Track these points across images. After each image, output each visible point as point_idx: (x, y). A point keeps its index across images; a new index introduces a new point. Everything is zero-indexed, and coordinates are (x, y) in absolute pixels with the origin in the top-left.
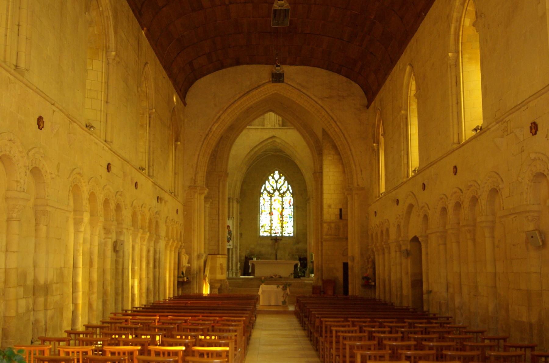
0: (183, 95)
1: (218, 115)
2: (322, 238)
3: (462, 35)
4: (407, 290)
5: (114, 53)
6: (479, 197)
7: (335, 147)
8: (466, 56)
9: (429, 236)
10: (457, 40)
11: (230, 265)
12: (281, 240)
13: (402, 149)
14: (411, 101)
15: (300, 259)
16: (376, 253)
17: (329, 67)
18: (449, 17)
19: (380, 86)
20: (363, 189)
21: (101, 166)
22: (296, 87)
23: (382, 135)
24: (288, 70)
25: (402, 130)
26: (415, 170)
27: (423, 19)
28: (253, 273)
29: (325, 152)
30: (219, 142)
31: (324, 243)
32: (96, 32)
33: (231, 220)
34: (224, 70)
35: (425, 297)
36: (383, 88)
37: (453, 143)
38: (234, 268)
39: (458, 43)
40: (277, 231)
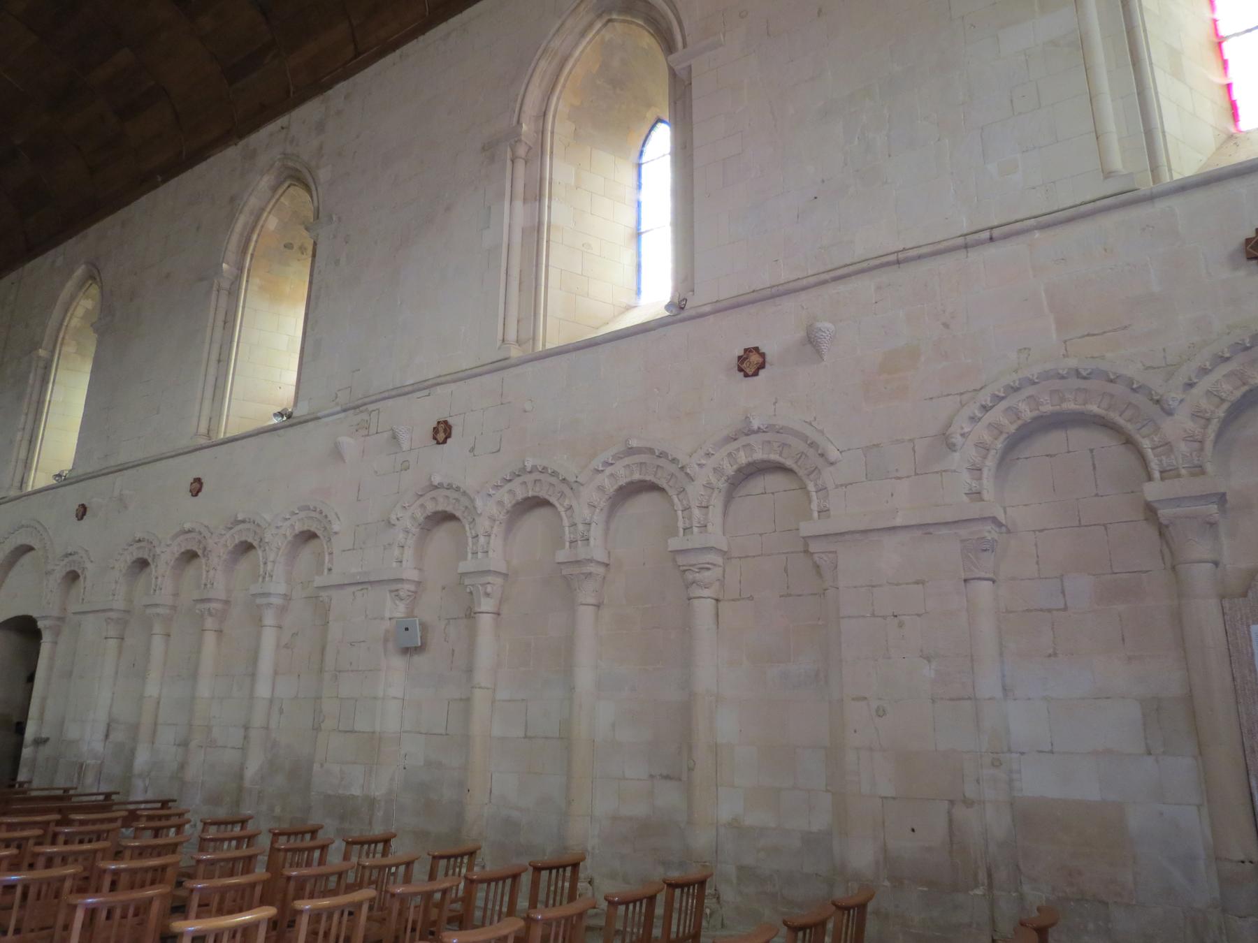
3: (256, 241)
8: (256, 281)
13: (21, 426)
14: (67, 337)
25: (29, 390)
27: (156, 187)
35: (27, 752)
37: (197, 434)
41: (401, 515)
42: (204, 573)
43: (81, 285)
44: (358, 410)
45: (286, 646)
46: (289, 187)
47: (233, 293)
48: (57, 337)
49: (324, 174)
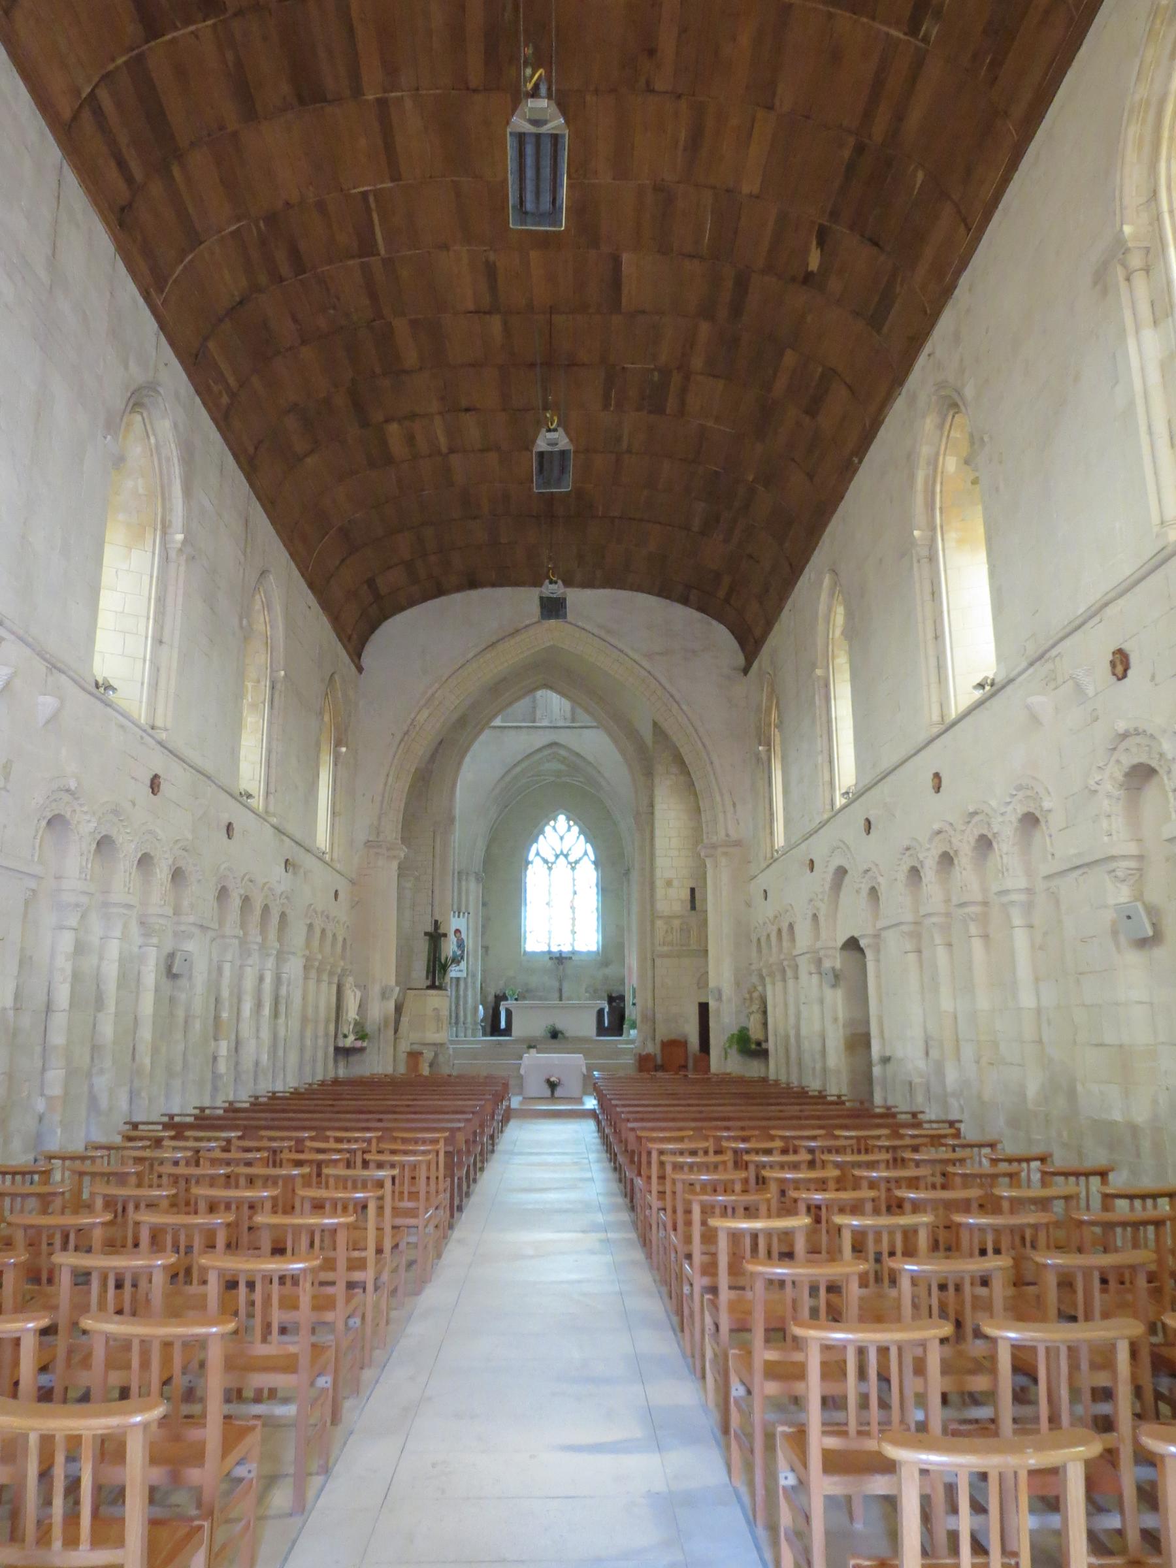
0: (356, 650)
1: (430, 692)
2: (653, 952)
3: (941, 491)
4: (836, 1058)
5: (180, 537)
6: (995, 837)
7: (679, 761)
8: (952, 536)
9: (884, 934)
10: (930, 506)
11: (462, 1014)
12: (571, 958)
15: (611, 999)
16: (768, 980)
17: (664, 591)
18: (910, 457)
19: (769, 625)
20: (738, 843)
21: (133, 778)
22: (595, 631)
23: (776, 726)
24: (578, 599)
26: (847, 793)
28: (508, 1031)
29: (659, 769)
30: (436, 750)
31: (658, 962)
32: (141, 491)
33: (464, 916)
34: (443, 599)
35: (877, 1070)
36: (776, 627)
38: (469, 1019)
39: (933, 509)
40: (562, 944)
41: (1100, 778)
42: (998, 858)
43: (832, 595)
44: (1043, 660)
45: (1041, 948)
46: (954, 416)
47: (932, 558)
48: (828, 651)
49: (969, 392)
